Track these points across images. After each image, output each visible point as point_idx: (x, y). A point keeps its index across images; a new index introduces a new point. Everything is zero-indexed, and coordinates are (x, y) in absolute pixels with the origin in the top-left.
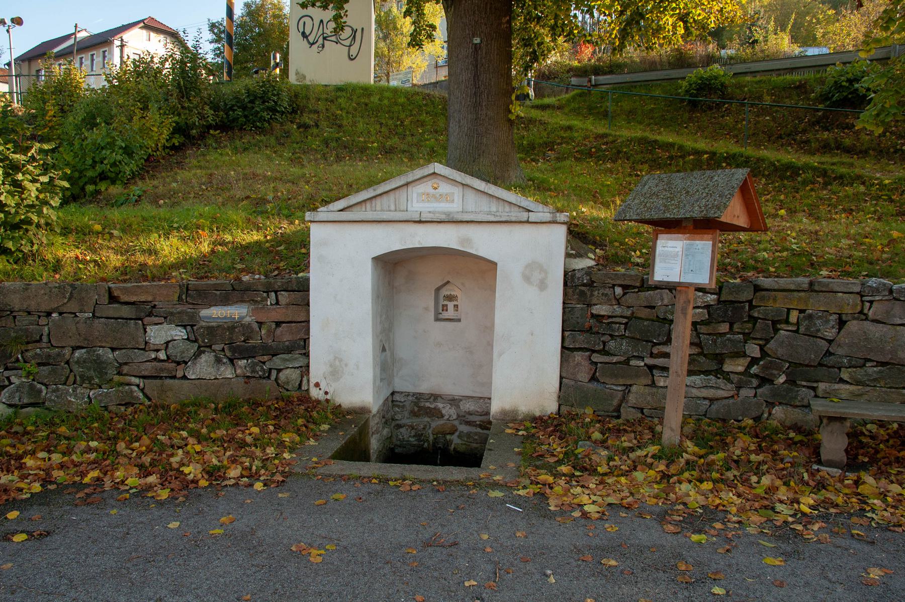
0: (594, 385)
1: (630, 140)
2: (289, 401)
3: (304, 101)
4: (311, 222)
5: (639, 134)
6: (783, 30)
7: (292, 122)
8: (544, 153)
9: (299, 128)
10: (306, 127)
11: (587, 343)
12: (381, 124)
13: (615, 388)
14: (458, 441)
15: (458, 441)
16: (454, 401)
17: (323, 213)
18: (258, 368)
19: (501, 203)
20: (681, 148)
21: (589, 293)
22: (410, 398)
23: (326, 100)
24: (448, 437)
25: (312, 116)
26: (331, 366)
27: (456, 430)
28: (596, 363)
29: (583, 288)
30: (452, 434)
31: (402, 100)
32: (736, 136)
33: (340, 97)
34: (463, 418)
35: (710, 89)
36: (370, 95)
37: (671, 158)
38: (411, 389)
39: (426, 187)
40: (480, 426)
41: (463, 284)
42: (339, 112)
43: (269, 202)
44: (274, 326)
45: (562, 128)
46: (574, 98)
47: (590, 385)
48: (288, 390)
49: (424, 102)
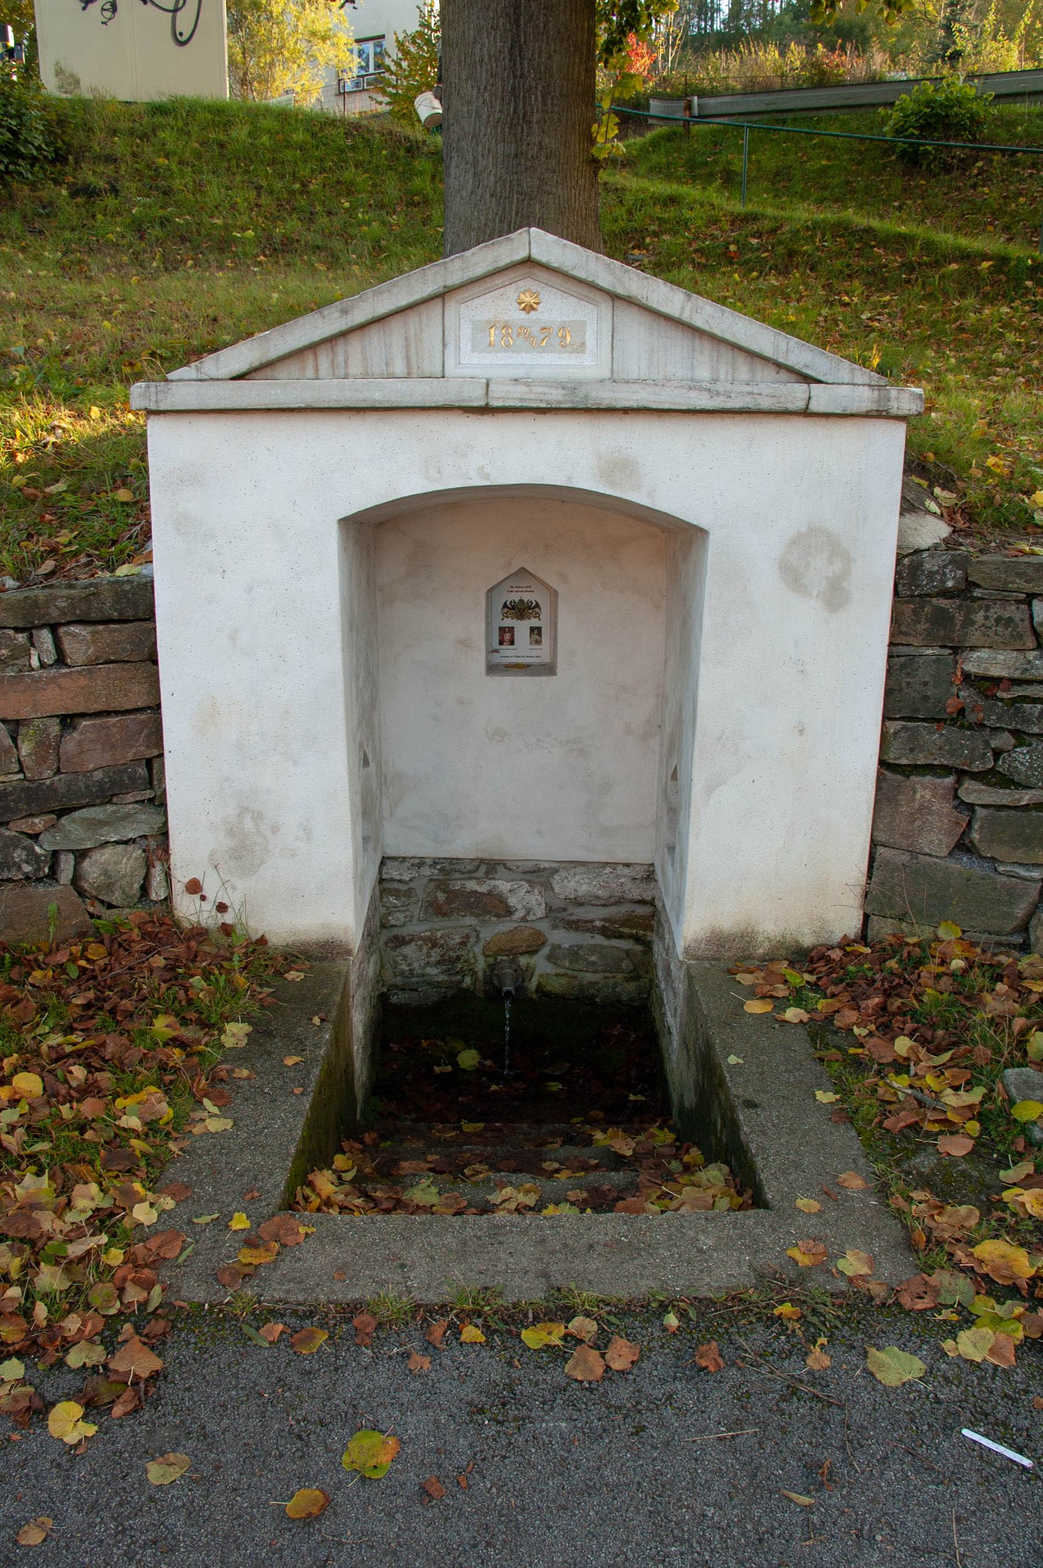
0: (963, 864)
1: (815, 227)
2: (116, 942)
3: (82, 135)
4: (150, 413)
5: (828, 215)
6: (1010, 35)
7: (57, 182)
8: (626, 253)
9: (74, 194)
10: (89, 193)
11: (952, 753)
12: (259, 188)
13: (1022, 872)
14: (549, 969)
15: (549, 969)
16: (538, 875)
17: (185, 386)
18: (19, 855)
19: (726, 354)
20: (929, 246)
21: (959, 618)
22: (426, 871)
23: (132, 133)
24: (523, 961)
25: (101, 168)
26: (231, 833)
27: (543, 944)
28: (971, 807)
29: (943, 603)
30: (533, 952)
31: (299, 137)
32: (1007, 229)
33: (163, 127)
34: (561, 915)
35: (947, 127)
36: (228, 125)
37: (909, 267)
38: (426, 848)
39: (500, 305)
40: (604, 932)
41: (562, 576)
42: (161, 161)
43: (17, 362)
44: (55, 728)
45: (656, 200)
46: (655, 144)
47: (952, 865)
48: (110, 906)
49: (349, 142)
